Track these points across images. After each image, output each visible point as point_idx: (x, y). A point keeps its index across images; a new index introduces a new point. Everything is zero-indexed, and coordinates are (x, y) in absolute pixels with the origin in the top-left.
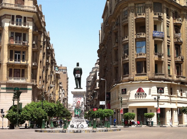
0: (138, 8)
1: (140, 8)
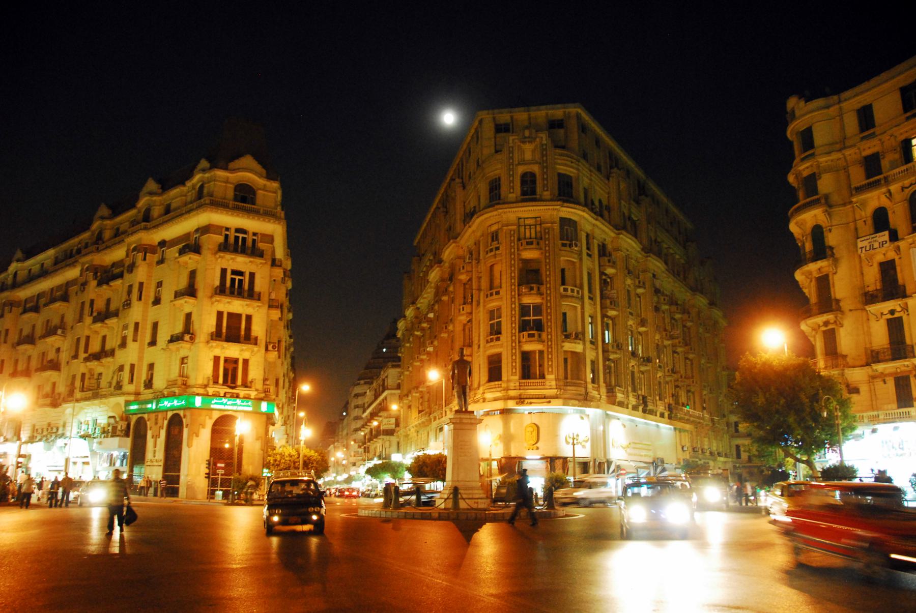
0: (525, 228)
1: (530, 228)
